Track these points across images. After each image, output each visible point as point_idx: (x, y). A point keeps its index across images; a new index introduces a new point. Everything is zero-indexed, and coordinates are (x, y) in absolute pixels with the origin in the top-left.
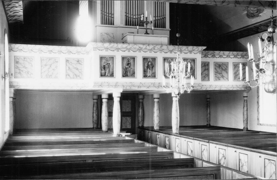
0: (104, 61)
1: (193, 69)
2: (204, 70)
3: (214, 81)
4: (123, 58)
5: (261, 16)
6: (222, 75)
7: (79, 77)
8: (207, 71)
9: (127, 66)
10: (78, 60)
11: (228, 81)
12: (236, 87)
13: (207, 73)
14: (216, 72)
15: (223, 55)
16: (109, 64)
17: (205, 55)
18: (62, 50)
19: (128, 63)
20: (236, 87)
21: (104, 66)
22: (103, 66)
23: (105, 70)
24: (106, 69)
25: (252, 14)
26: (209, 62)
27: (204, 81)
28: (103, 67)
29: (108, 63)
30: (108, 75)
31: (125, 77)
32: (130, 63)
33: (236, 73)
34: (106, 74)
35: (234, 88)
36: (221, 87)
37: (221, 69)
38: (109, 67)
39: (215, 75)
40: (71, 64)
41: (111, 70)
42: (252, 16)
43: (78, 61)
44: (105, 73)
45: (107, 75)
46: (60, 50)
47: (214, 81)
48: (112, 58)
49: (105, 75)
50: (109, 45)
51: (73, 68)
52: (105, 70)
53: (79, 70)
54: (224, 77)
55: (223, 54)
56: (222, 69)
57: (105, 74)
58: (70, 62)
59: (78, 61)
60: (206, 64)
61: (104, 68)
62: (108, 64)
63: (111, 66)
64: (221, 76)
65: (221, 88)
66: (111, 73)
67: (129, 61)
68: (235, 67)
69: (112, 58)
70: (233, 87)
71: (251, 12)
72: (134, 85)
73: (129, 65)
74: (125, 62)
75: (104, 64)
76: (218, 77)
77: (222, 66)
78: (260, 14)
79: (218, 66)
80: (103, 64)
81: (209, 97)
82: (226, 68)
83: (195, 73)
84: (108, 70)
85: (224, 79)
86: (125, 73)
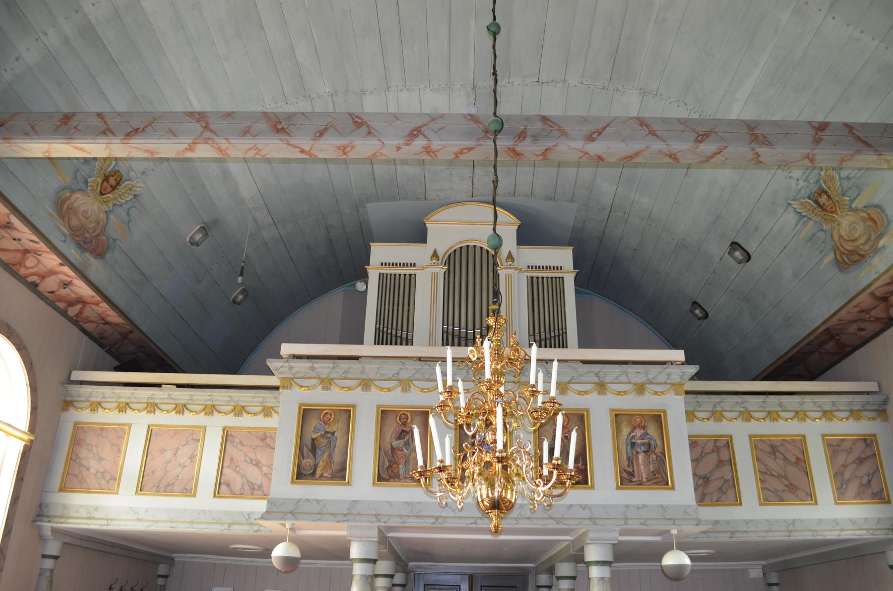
0: (314, 422)
1: (657, 451)
2: (718, 466)
3: (761, 504)
4: (384, 414)
5: (884, 246)
6: (787, 483)
7: (260, 492)
8: (728, 468)
9: (398, 442)
10: (265, 433)
11: (816, 503)
12: (852, 527)
13: (728, 476)
14: (764, 474)
15: (780, 409)
16: (333, 434)
17: (713, 413)
18: (216, 403)
19: (403, 431)
20: (852, 527)
21: (313, 440)
22: (309, 442)
23: (314, 455)
24: (319, 453)
25: (852, 253)
26: (731, 437)
27: (720, 505)
28: (310, 446)
29: (327, 432)
30: (326, 475)
31: (387, 480)
32: (408, 429)
33: (842, 474)
34: (318, 472)
35: (842, 530)
36: (791, 528)
37: (781, 462)
38: (330, 445)
39: (762, 481)
40: (240, 446)
41: (337, 457)
42: (856, 262)
43: (264, 439)
44: (315, 467)
45: (321, 476)
46: (210, 403)
47: (761, 504)
48: (347, 413)
49: (313, 474)
50: (334, 368)
51: (246, 461)
52: (314, 455)
53: (264, 468)
54: (798, 488)
55: (780, 405)
56: (786, 459)
57: (315, 470)
58: (237, 440)
59: (264, 439)
60: (719, 444)
61: (314, 449)
62: (329, 435)
63: (338, 443)
64: (787, 486)
65: (790, 531)
66: (336, 467)
67: (404, 424)
68: (834, 450)
69: (347, 413)
70: (838, 528)
71: (849, 248)
72: (421, 514)
73: (407, 437)
74: (392, 426)
75: (314, 437)
76: (775, 492)
77: (780, 449)
78: (881, 243)
79: (768, 449)
80: (311, 434)
81: (774, 581)
82: (801, 456)
83: (665, 464)
84: (326, 456)
85: (797, 496)
86: (390, 466)
